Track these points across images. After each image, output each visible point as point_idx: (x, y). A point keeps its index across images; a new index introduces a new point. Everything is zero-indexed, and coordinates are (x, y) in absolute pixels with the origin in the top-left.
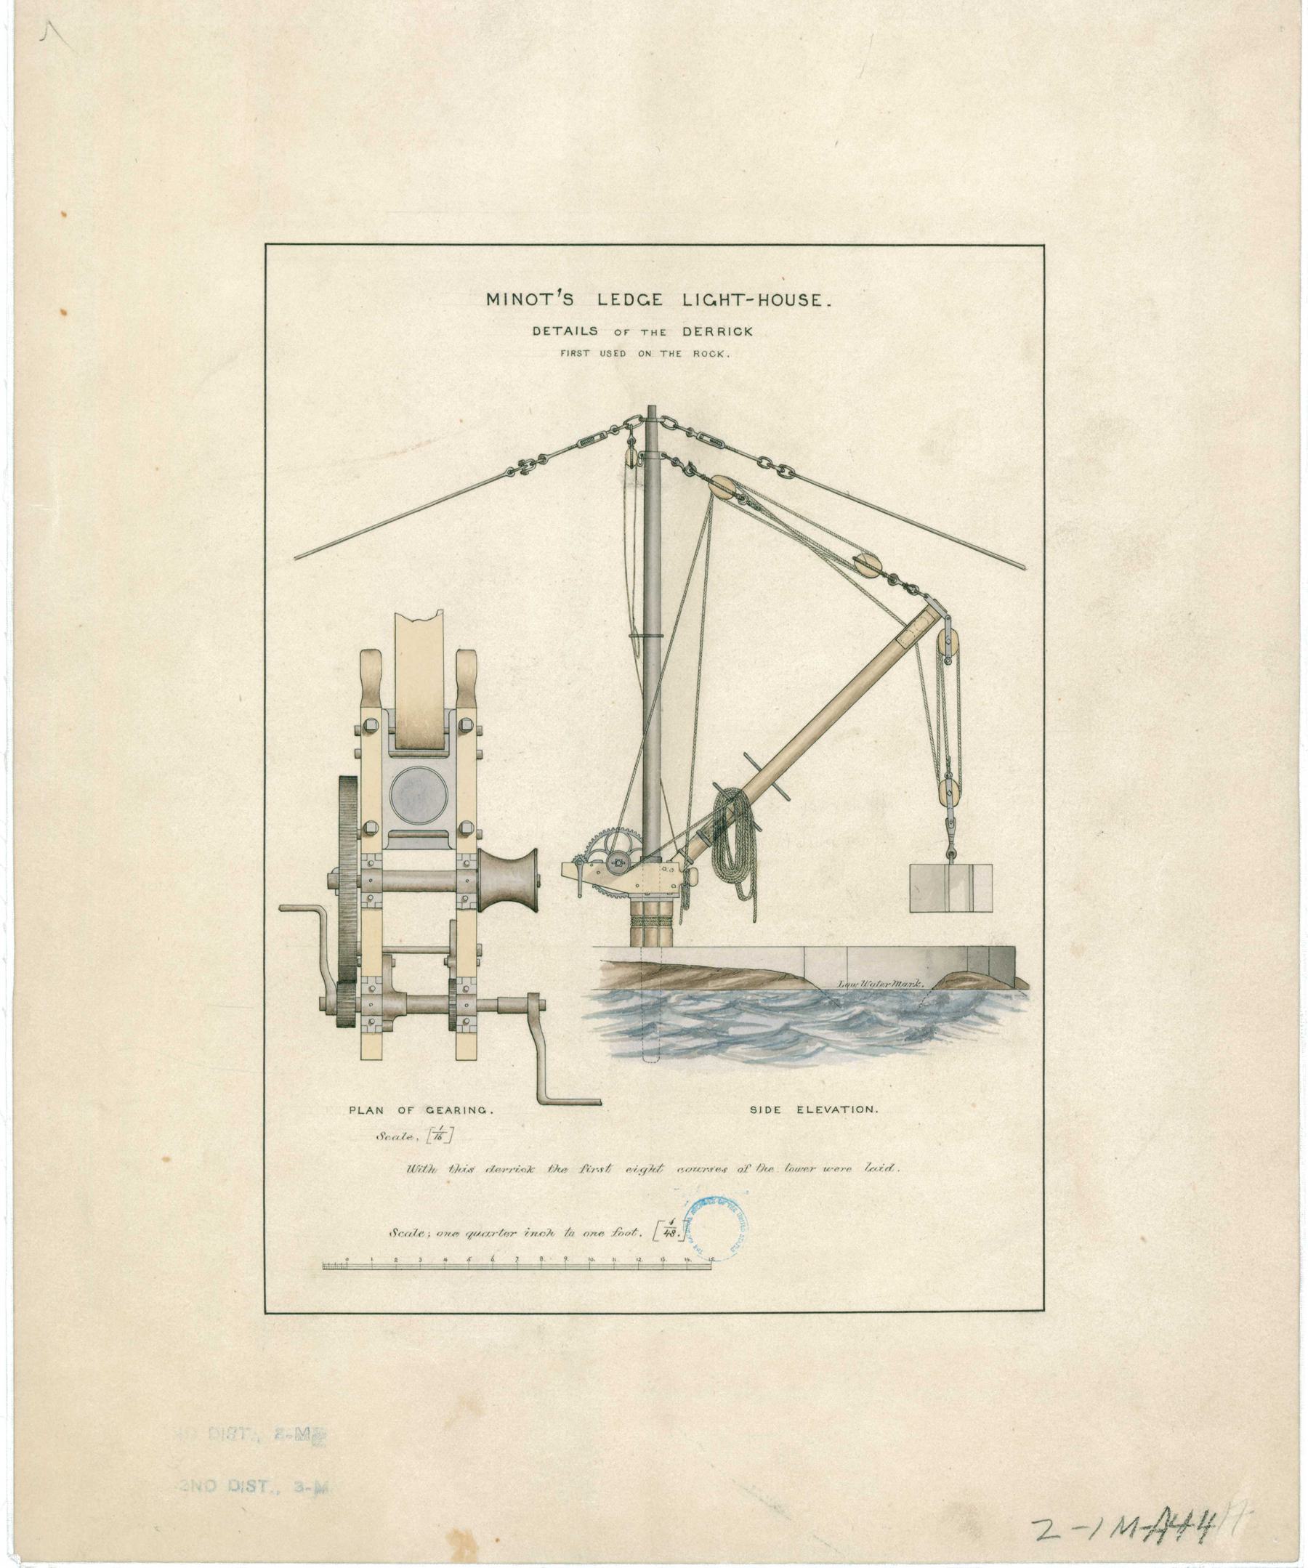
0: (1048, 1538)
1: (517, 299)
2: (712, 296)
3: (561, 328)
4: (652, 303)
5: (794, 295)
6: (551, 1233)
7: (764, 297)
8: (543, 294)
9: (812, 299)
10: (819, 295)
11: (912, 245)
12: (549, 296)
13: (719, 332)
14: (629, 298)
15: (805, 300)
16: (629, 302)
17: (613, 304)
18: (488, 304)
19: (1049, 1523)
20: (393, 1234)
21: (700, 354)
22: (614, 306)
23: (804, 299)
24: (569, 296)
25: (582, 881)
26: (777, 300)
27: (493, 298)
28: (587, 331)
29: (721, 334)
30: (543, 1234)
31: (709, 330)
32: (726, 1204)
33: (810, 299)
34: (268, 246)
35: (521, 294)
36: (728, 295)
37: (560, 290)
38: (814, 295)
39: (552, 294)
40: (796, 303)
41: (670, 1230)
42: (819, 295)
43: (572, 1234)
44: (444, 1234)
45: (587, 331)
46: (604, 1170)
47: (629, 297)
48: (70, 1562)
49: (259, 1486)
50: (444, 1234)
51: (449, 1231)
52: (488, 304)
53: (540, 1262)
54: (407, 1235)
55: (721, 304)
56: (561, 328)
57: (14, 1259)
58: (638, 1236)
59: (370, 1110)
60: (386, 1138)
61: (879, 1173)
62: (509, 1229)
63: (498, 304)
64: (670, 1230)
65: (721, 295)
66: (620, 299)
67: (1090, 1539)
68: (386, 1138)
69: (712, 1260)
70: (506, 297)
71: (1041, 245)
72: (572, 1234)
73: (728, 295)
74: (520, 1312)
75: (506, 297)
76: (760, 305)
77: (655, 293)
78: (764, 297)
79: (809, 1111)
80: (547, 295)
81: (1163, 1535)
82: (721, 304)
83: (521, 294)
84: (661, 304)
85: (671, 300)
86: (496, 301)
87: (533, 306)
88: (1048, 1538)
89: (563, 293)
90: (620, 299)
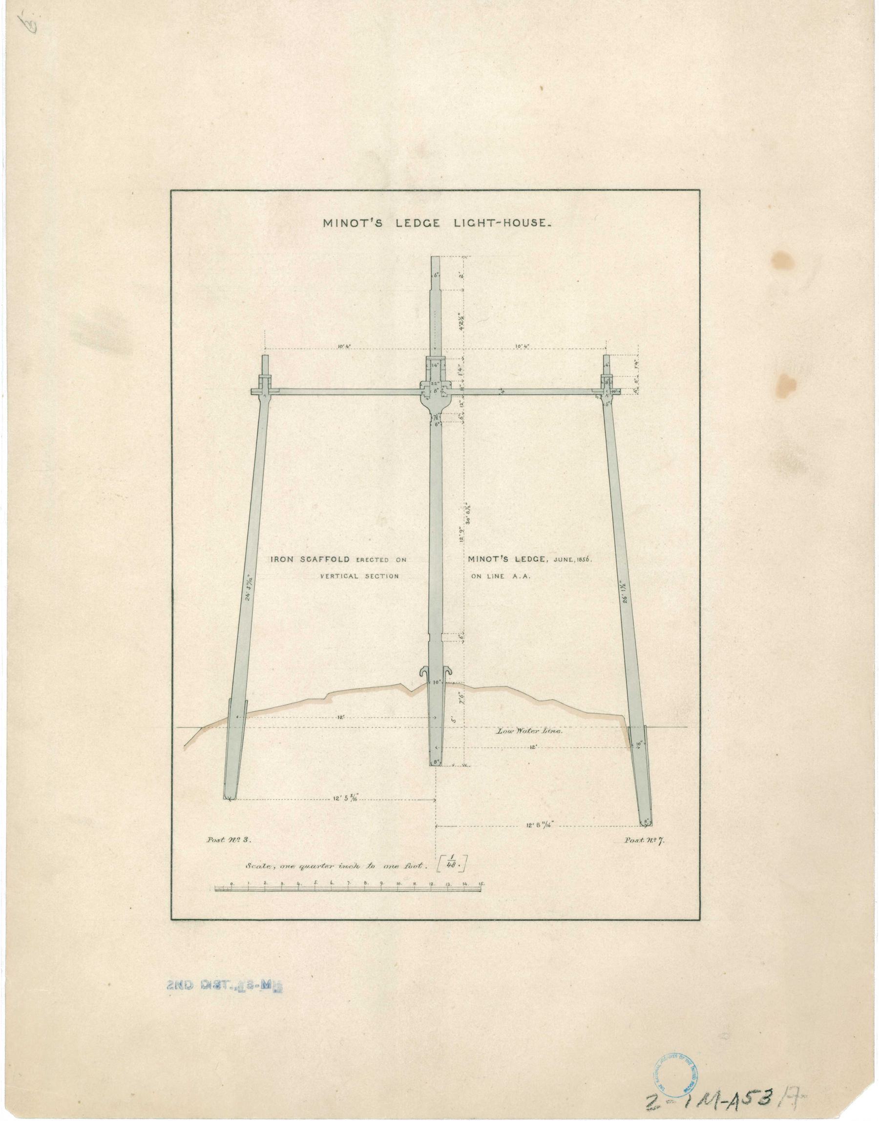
1: (344, 223)
3: (494, 220)
6: (357, 866)
8: (362, 220)
10: (544, 219)
11: (492, 190)
13: (275, 559)
15: (380, 223)
20: (248, 866)
21: (279, 560)
23: (380, 223)
24: (378, 224)
26: (516, 223)
28: (342, 559)
30: (351, 867)
31: (277, 558)
32: (685, 1059)
33: (538, 222)
35: (347, 220)
36: (484, 220)
37: (372, 219)
38: (434, 220)
39: (368, 220)
41: (452, 863)
42: (544, 219)
43: (373, 867)
44: (285, 867)
45: (342, 559)
46: (220, 841)
47: (417, 221)
49: (222, 984)
50: (285, 867)
51: (288, 865)
54: (258, 867)
56: (494, 220)
57: (6, 882)
59: (351, 576)
61: (263, 869)
63: (332, 226)
64: (452, 863)
69: (481, 884)
70: (464, 224)
72: (373, 867)
73: (484, 220)
74: (393, 918)
75: (464, 224)
80: (364, 220)
83: (347, 220)
84: (342, 226)
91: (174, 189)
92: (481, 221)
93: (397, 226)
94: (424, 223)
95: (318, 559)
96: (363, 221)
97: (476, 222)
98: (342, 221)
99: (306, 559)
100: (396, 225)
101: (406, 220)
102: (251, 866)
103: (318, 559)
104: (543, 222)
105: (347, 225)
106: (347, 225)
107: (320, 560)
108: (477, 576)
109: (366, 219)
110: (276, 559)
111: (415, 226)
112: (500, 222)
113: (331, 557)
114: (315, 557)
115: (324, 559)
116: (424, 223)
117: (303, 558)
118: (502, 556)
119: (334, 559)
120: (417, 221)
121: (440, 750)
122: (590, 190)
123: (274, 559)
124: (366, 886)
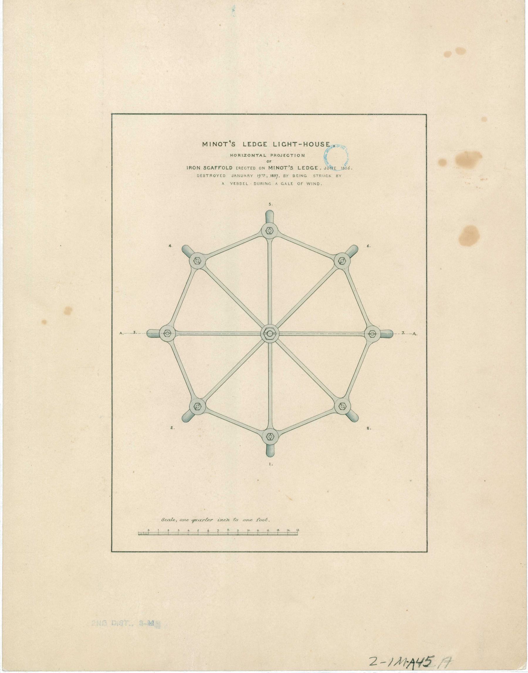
0: (373, 665)
2: (285, 143)
4: (314, 168)
5: (316, 142)
7: (306, 143)
9: (263, 144)
10: (266, 142)
12: (226, 143)
13: (190, 168)
14: (308, 167)
15: (324, 145)
16: (308, 168)
17: (248, 146)
18: (203, 146)
19: (375, 658)
20: (163, 520)
21: (192, 168)
22: (249, 147)
25: (218, 532)
27: (205, 144)
28: (228, 168)
29: (275, 156)
32: (340, 147)
33: (296, 176)
34: (425, 115)
35: (216, 143)
36: (291, 143)
37: (230, 141)
39: (227, 142)
40: (320, 145)
42: (266, 142)
45: (228, 168)
47: (308, 167)
48: (429, 670)
49: (124, 623)
52: (203, 146)
53: (227, 531)
55: (288, 146)
58: (268, 521)
60: (165, 520)
62: (210, 518)
63: (272, 169)
65: (288, 143)
66: (251, 144)
67: (388, 666)
68: (165, 520)
71: (425, 115)
73: (291, 143)
75: (210, 143)
76: (304, 146)
77: (249, 142)
78: (306, 143)
79: (227, 168)
80: (225, 143)
81: (414, 664)
82: (288, 146)
83: (216, 143)
85: (269, 144)
86: (206, 144)
87: (311, 147)
88: (373, 665)
89: (290, 166)
90: (305, 168)
91: (427, 116)
92: (289, 143)
93: (426, 115)
94: (219, 144)
95: (214, 167)
96: (294, 143)
97: (287, 144)
98: (214, 143)
99: (207, 168)
100: (427, 115)
101: (248, 143)
102: (164, 520)
103: (214, 167)
104: (249, 144)
105: (216, 145)
106: (216, 145)
107: (215, 168)
108: (196, 168)
109: (226, 142)
110: (190, 167)
111: (253, 146)
112: (301, 144)
113: (222, 167)
114: (212, 167)
115: (217, 168)
116: (219, 144)
117: (205, 167)
118: (289, 166)
119: (223, 168)
120: (254, 143)
121: (433, 160)
122: (112, 523)
123: (188, 167)
124: (149, 531)
